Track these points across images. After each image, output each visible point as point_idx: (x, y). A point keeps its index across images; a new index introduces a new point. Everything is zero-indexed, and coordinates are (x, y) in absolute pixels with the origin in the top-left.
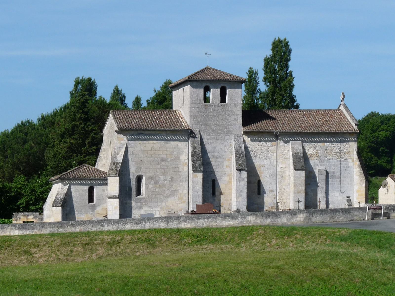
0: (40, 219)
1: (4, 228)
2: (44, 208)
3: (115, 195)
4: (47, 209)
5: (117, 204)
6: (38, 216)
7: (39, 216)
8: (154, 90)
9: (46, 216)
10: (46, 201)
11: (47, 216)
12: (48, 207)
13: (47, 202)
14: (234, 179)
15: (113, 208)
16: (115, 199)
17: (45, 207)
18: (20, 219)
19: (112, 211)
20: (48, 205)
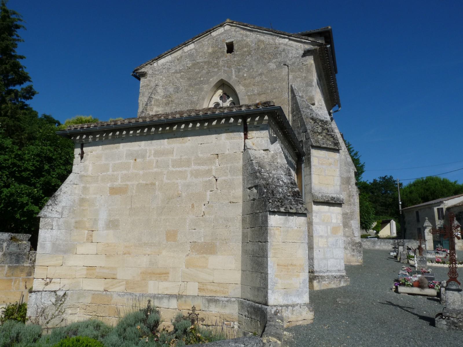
0: (11, 254)
1: (11, 280)
2: (45, 217)
3: (334, 196)
4: (54, 223)
5: (339, 222)
6: (5, 244)
7: (8, 245)
8: (419, 222)
9: (48, 245)
10: (57, 193)
11: (54, 244)
12: (62, 214)
13: (59, 199)
14: (336, 281)
15: (329, 230)
16: (332, 208)
17: (49, 215)
18: (353, 255)
19: (327, 237)
20: (63, 208)
